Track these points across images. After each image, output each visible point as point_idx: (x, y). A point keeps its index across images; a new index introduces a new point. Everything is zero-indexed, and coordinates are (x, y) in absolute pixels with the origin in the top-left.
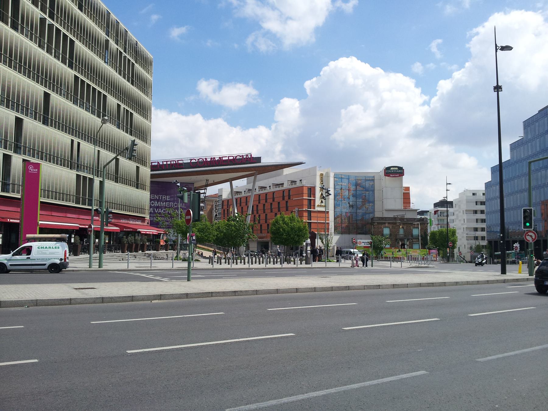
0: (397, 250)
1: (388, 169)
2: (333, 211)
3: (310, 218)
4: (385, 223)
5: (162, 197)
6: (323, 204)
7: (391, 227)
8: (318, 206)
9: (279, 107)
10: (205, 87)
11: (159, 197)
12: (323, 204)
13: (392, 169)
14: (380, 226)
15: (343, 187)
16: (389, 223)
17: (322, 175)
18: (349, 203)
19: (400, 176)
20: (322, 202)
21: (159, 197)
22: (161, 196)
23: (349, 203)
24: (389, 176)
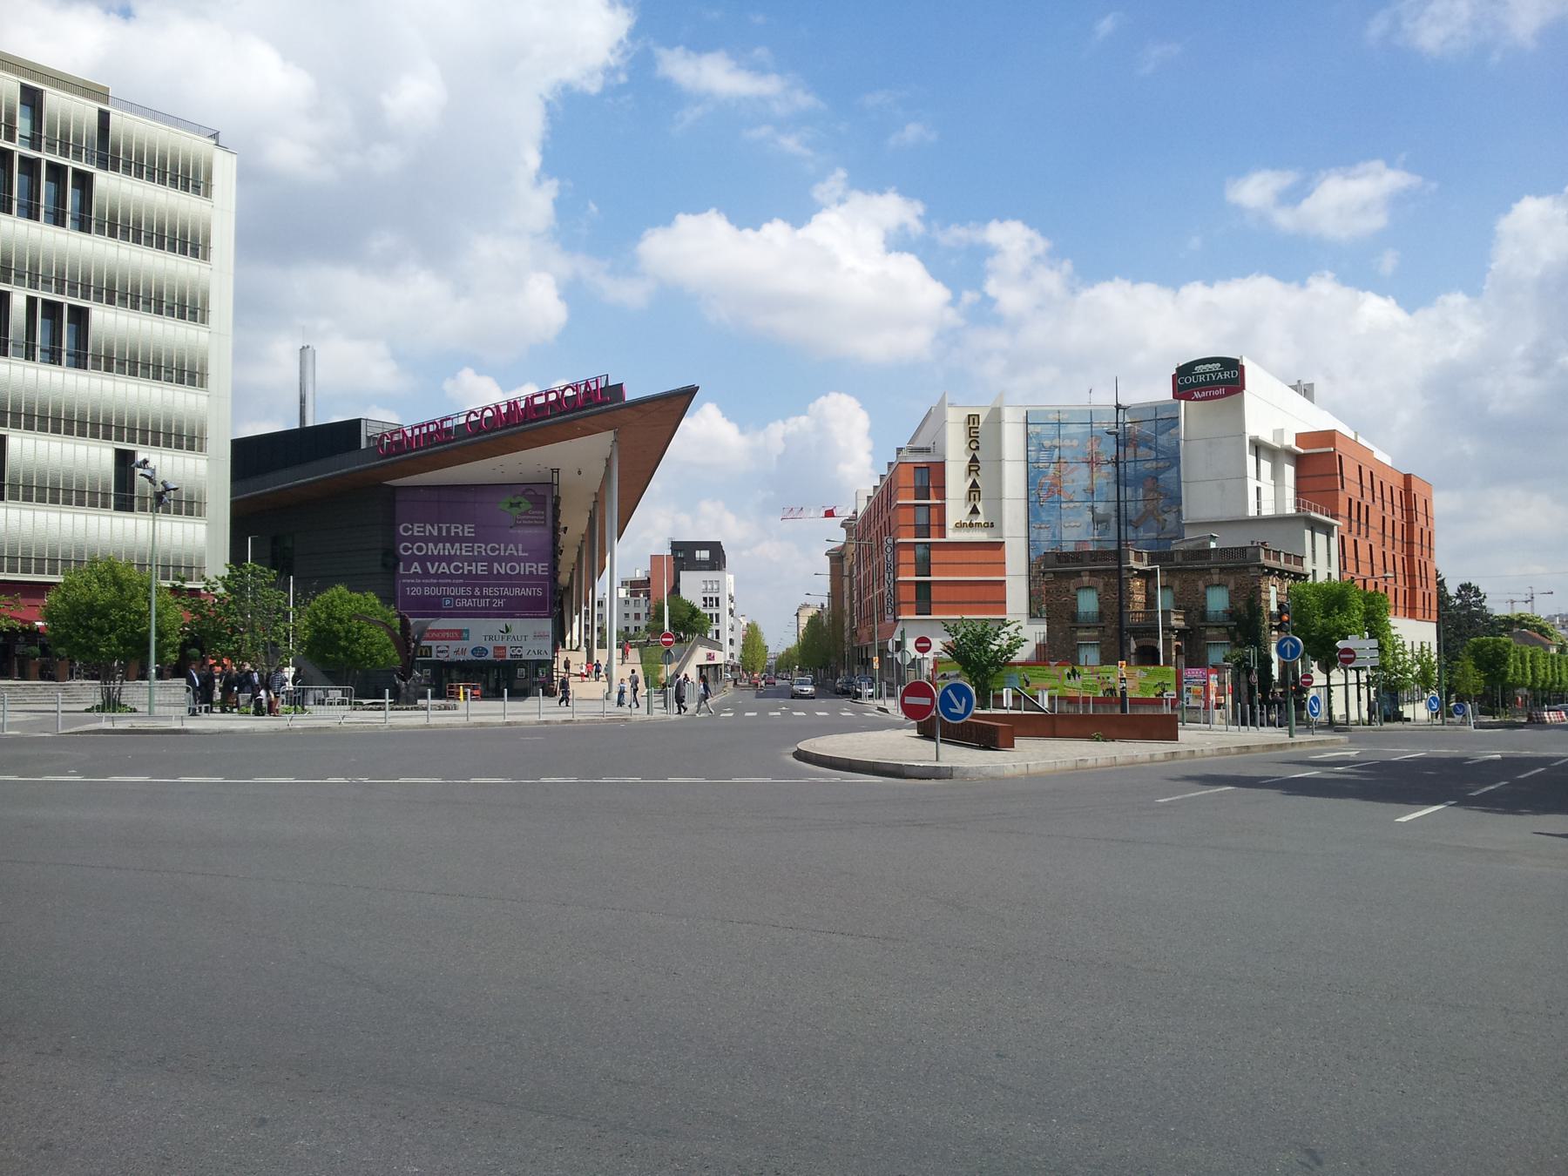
0: (1067, 670)
1: (1184, 371)
2: (1023, 543)
3: (924, 566)
4: (1078, 574)
5: (448, 530)
6: (981, 519)
7: (1101, 588)
8: (960, 526)
9: (1506, 225)
10: (1255, 191)
11: (440, 529)
12: (981, 519)
13: (1199, 369)
14: (1064, 584)
15: (1067, 454)
16: (1093, 573)
17: (972, 419)
18: (1092, 509)
19: (1229, 393)
20: (975, 511)
21: (440, 529)
22: (444, 527)
23: (1092, 509)
24: (1188, 397)
